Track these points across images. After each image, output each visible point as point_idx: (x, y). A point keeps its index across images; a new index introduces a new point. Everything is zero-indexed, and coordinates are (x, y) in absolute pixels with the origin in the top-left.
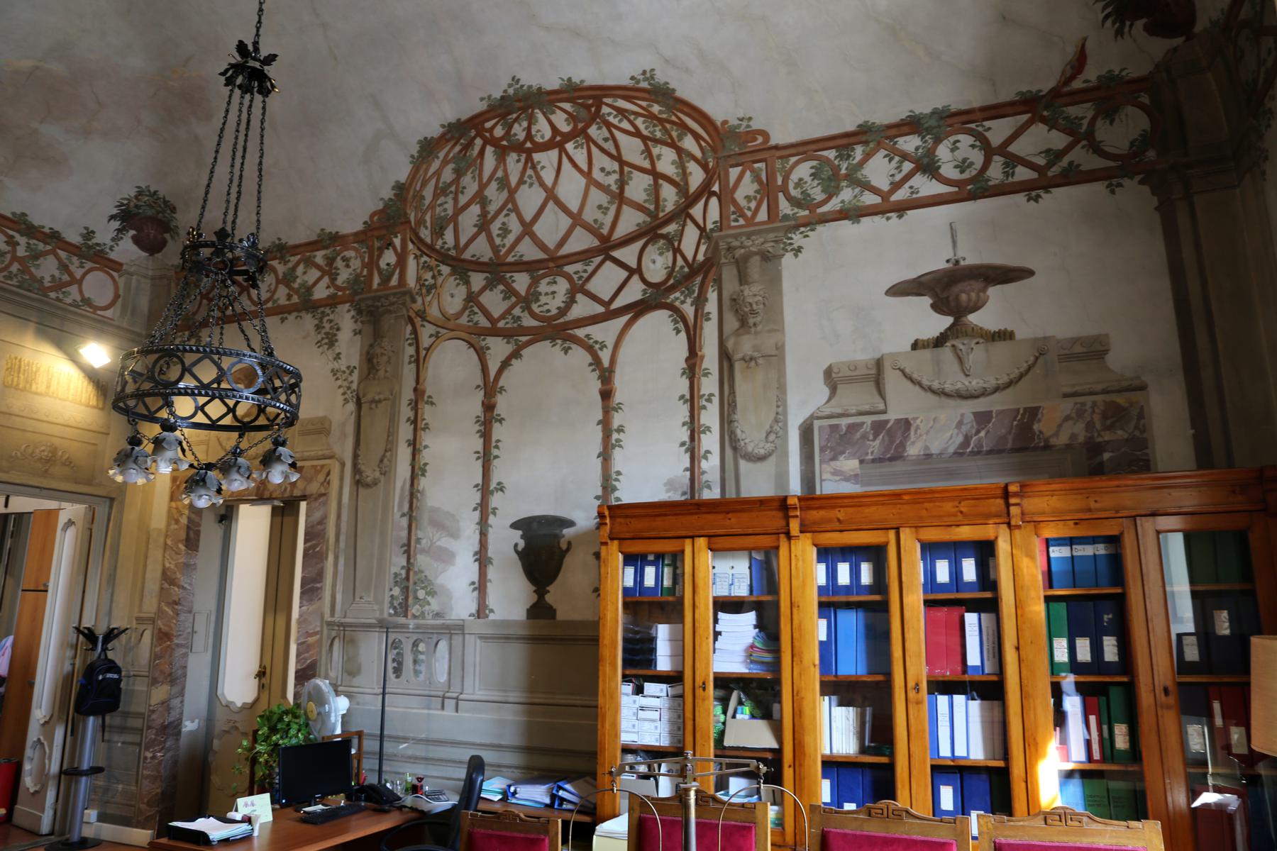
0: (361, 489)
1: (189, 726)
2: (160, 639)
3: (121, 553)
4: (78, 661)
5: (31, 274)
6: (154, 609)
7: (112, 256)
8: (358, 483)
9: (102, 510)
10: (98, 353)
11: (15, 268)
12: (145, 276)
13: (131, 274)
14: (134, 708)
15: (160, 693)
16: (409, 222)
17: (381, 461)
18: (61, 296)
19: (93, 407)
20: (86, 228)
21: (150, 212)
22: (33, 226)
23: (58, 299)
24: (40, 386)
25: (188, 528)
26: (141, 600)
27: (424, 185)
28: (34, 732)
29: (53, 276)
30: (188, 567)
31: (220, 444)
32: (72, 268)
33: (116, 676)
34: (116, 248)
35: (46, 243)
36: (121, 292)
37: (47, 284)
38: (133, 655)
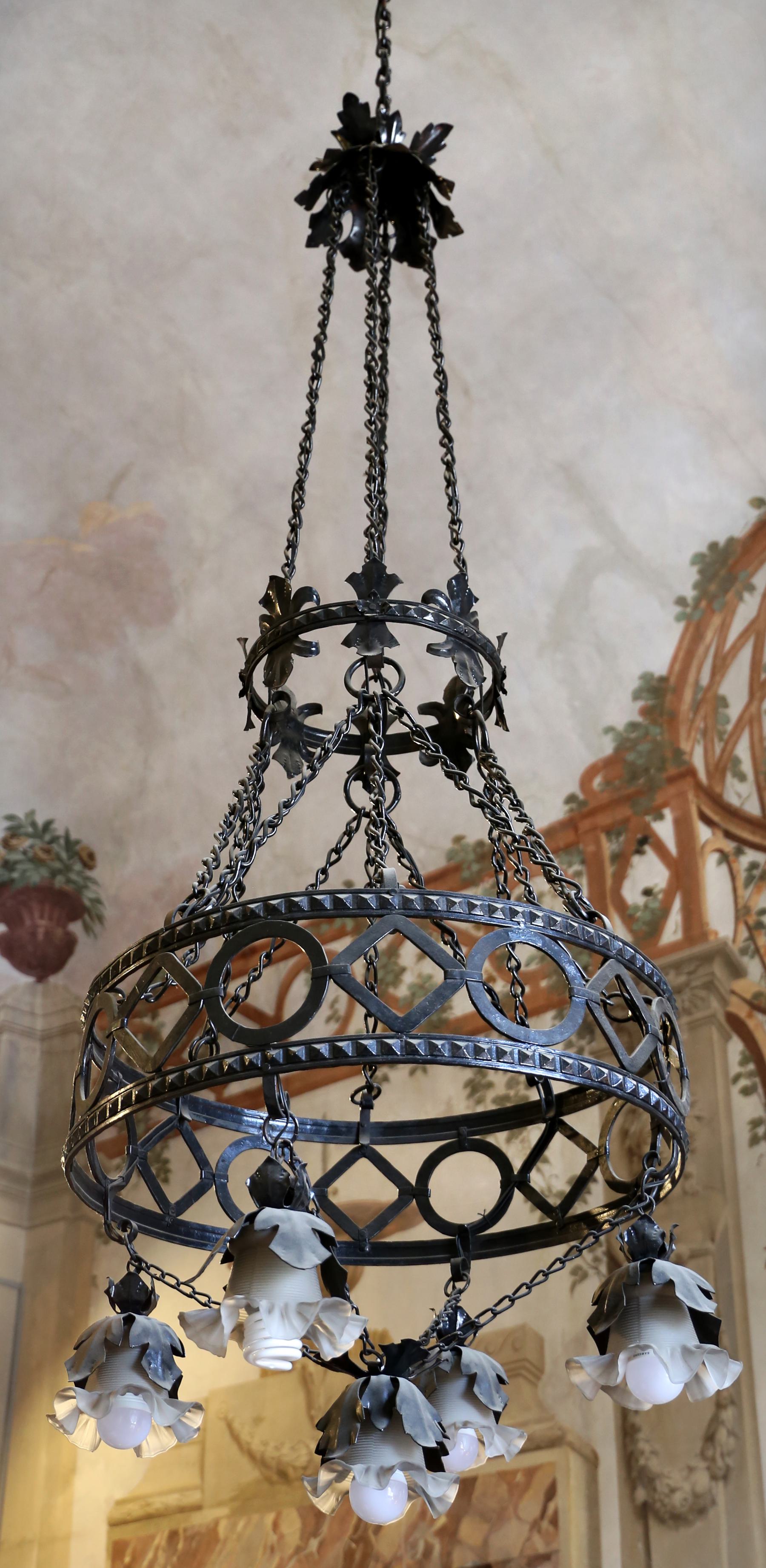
0: (655, 1530)
8: (645, 1513)
12: (28, 1033)
16: (692, 772)
17: (710, 1438)
21: (36, 876)
27: (720, 667)
31: (235, 1437)
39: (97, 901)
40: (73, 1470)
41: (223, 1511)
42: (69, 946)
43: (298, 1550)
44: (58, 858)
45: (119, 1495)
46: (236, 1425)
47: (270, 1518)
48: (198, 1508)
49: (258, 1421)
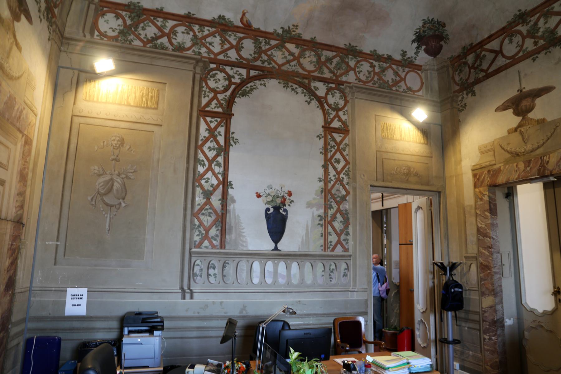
1: (509, 322)
2: (482, 269)
3: (449, 221)
4: (436, 281)
5: (383, 80)
6: (475, 251)
7: (417, 62)
9: (435, 199)
10: (421, 113)
11: (376, 78)
12: (433, 70)
13: (427, 70)
14: (471, 309)
15: (487, 301)
18: (398, 88)
19: (423, 144)
20: (402, 51)
21: (431, 33)
22: (379, 55)
23: (397, 90)
24: (397, 136)
25: (489, 202)
26: (466, 247)
28: (418, 316)
29: (392, 79)
30: (493, 226)
32: (400, 73)
33: (460, 290)
34: (417, 58)
35: (386, 63)
36: (424, 81)
37: (391, 84)
38: (470, 277)
39: (447, 35)
40: (461, 161)
41: (502, 164)
42: (441, 47)
43: (524, 170)
44: (436, 27)
45: (473, 164)
46: (503, 146)
47: (515, 165)
48: (495, 164)
49: (508, 144)
